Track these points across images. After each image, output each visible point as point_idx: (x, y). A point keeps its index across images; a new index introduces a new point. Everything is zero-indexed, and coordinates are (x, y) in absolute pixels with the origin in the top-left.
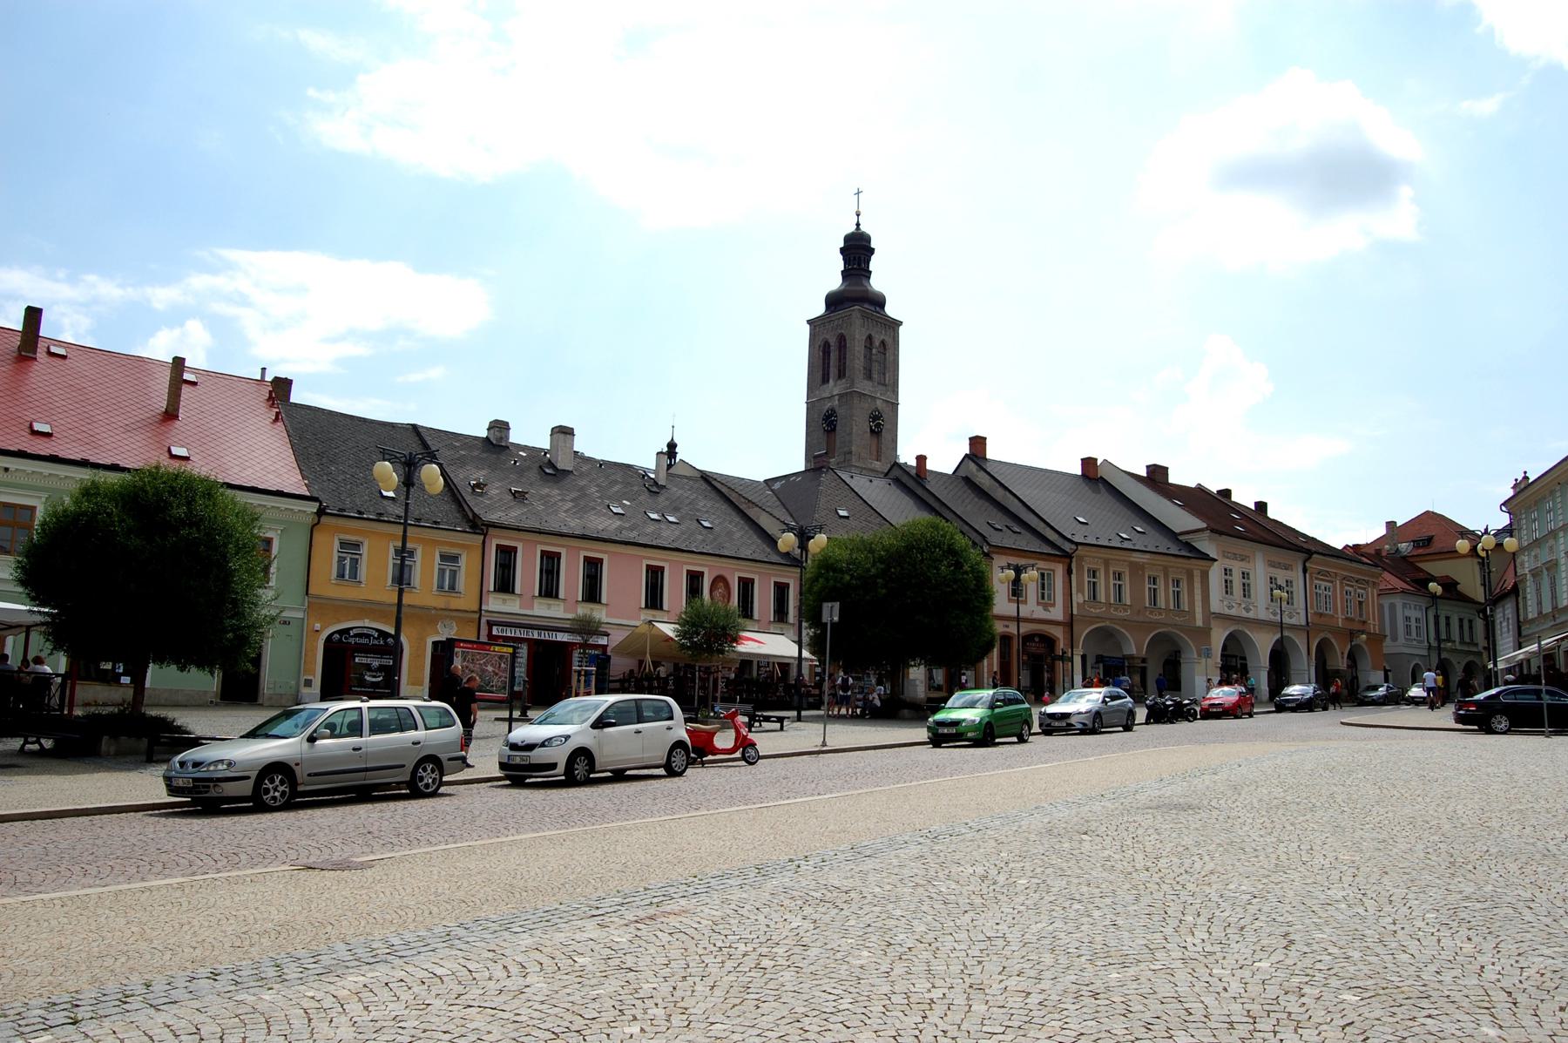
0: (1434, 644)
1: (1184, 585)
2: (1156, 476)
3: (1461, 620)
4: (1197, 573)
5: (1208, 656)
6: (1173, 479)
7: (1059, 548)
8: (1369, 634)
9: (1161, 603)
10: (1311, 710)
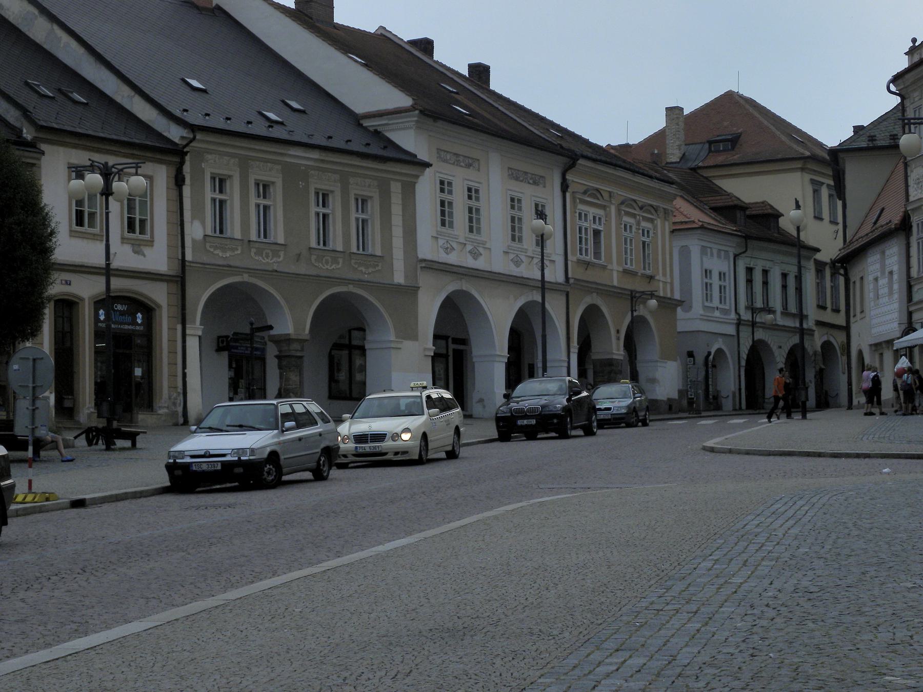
0: (746, 316)
1: (374, 207)
3: (784, 276)
4: (396, 188)
5: (409, 332)
7: (160, 136)
8: (659, 298)
9: (337, 242)
10: (563, 435)
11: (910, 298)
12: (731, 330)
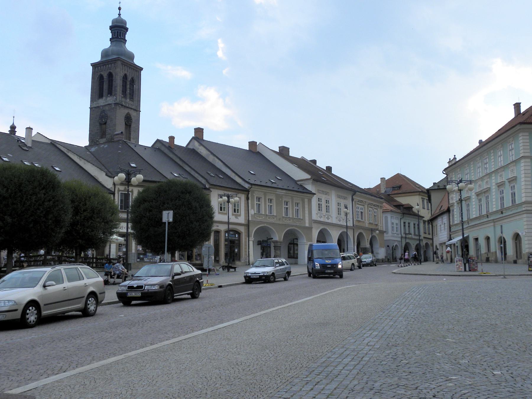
0: (404, 235)
2: (284, 152)
4: (306, 200)
6: (291, 154)
8: (379, 230)
11: (450, 231)
12: (400, 239)
